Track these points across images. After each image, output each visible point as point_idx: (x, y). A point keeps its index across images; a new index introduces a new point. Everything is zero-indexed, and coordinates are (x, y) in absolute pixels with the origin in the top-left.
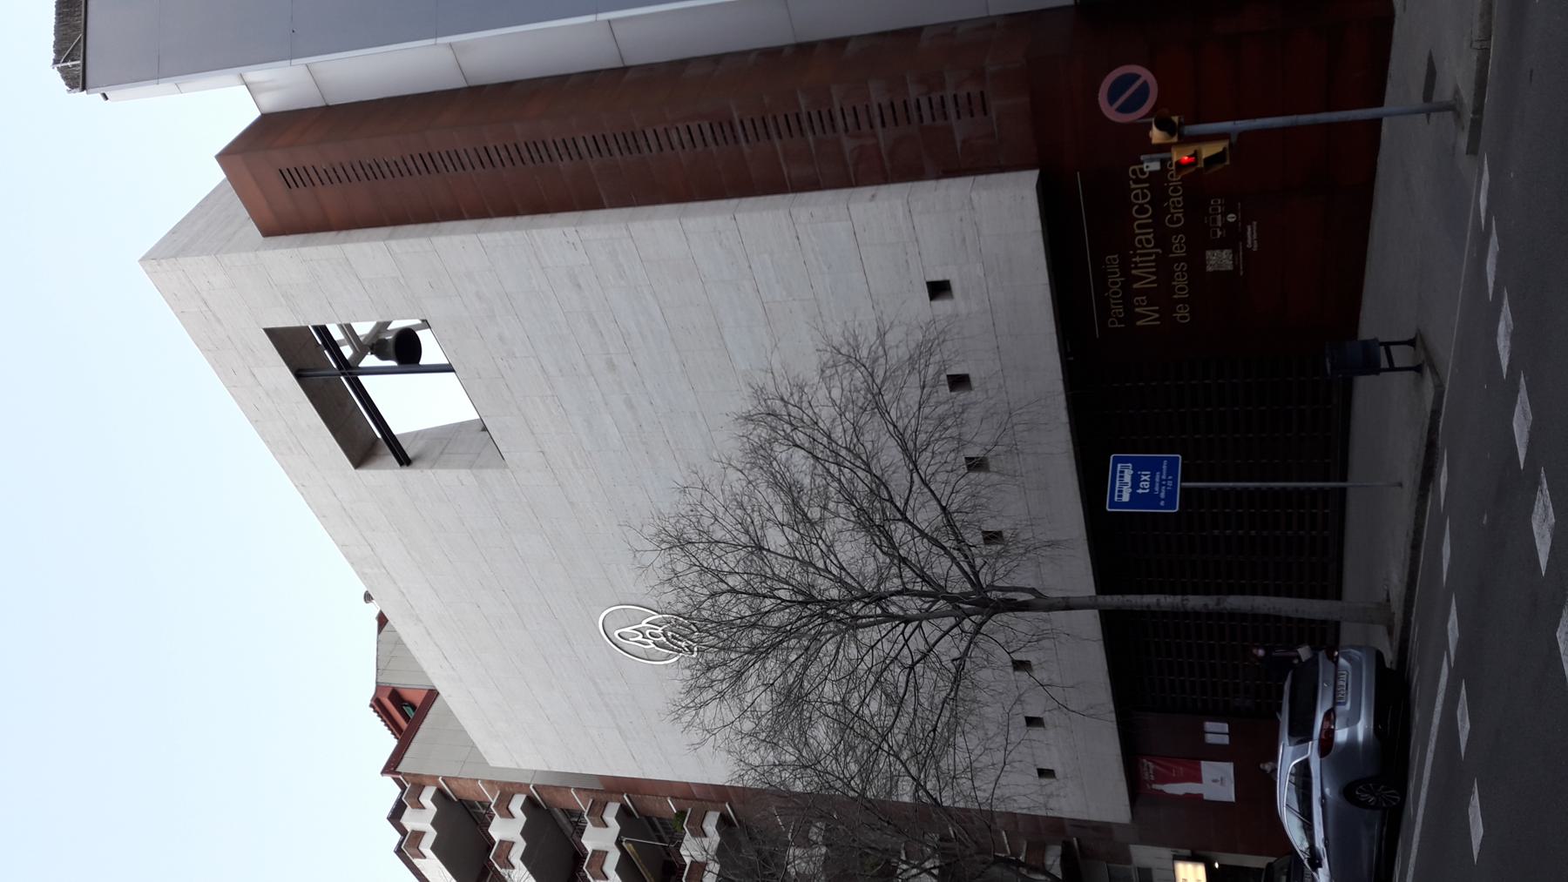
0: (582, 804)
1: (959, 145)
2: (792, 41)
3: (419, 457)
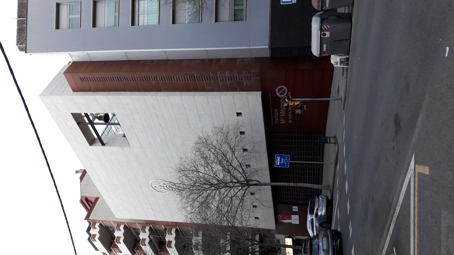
0: (139, 227)
2: (207, 58)
3: (106, 143)
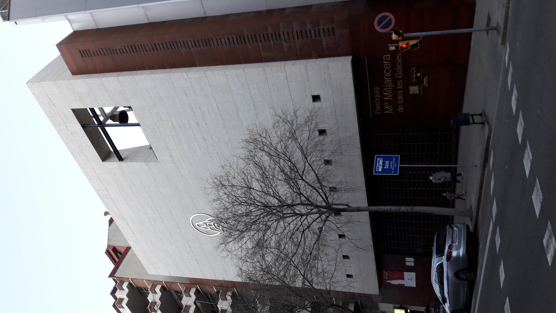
1: (324, 46)
2: (266, 9)
3: (126, 158)
